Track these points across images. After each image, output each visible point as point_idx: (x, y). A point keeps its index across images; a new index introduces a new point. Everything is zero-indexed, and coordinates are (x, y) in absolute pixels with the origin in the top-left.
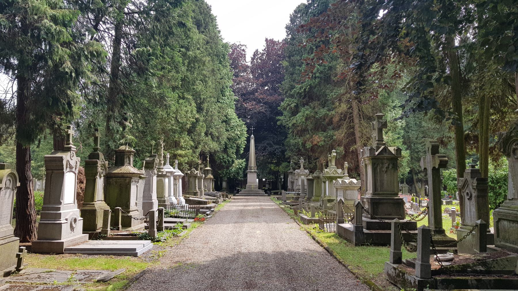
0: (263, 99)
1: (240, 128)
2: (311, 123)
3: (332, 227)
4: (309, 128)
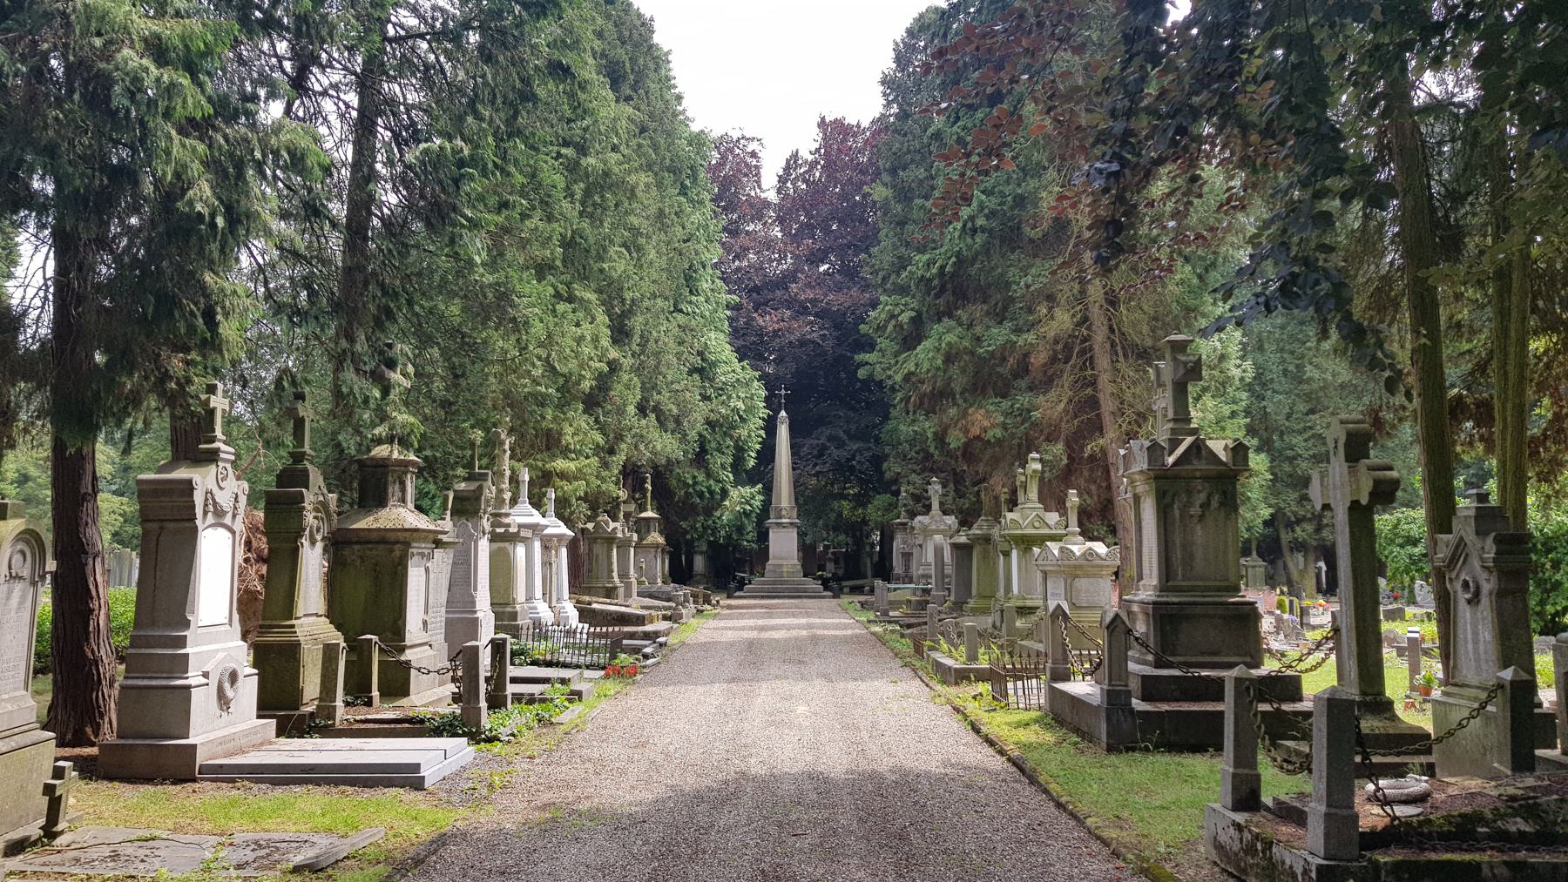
0: (814, 301)
1: (745, 391)
2: (963, 371)
3: (1032, 693)
4: (957, 387)
